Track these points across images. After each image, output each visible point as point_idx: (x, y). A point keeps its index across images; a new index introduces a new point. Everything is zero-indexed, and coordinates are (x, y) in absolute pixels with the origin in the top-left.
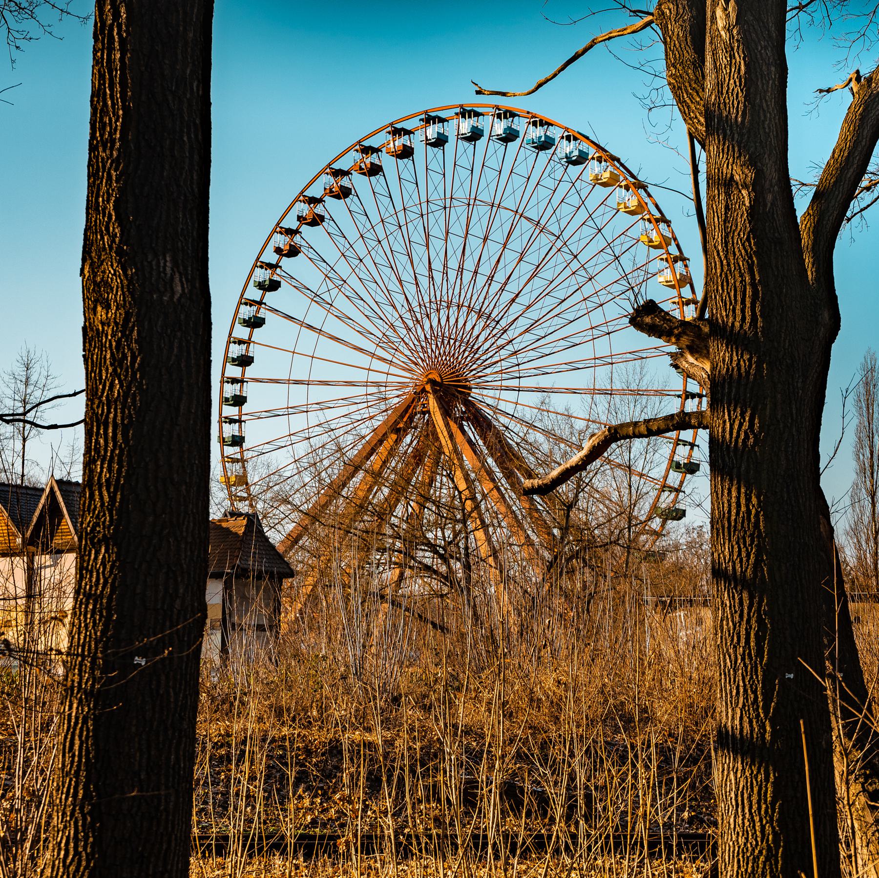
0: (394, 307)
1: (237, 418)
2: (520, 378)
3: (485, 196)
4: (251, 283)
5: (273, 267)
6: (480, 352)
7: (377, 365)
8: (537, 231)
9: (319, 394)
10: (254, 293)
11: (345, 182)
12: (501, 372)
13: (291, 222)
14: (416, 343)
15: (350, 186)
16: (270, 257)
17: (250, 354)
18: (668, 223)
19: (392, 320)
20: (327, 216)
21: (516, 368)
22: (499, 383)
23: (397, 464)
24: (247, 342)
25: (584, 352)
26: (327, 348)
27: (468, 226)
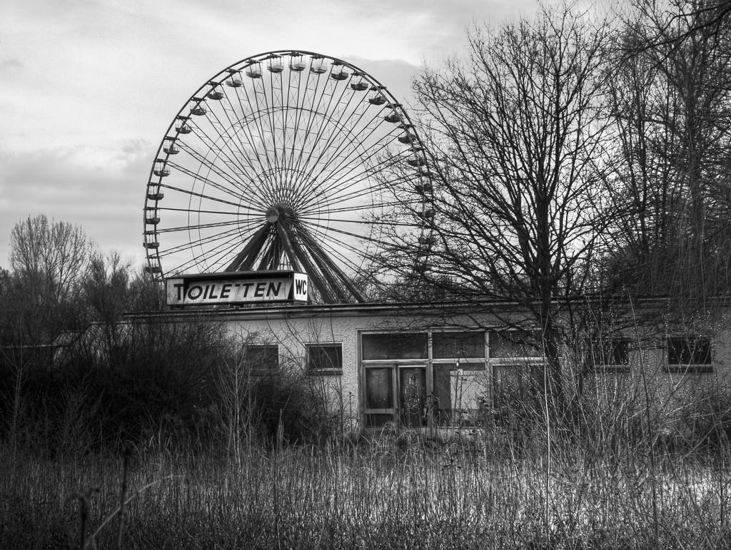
0: (253, 169)
1: (156, 255)
2: (371, 188)
3: (292, 104)
4: (162, 149)
5: (174, 139)
6: (299, 192)
7: (242, 210)
8: (326, 121)
9: (313, 161)
10: (163, 156)
11: (218, 89)
12: (250, 230)
13: (185, 113)
14: (268, 191)
15: (222, 92)
16: (173, 134)
17: (158, 217)
18: (400, 106)
19: (253, 178)
20: (208, 109)
21: (325, 200)
22: (317, 210)
23: (434, 272)
24: (159, 185)
25: (207, 247)
26: (207, 205)
27: (264, 146)
